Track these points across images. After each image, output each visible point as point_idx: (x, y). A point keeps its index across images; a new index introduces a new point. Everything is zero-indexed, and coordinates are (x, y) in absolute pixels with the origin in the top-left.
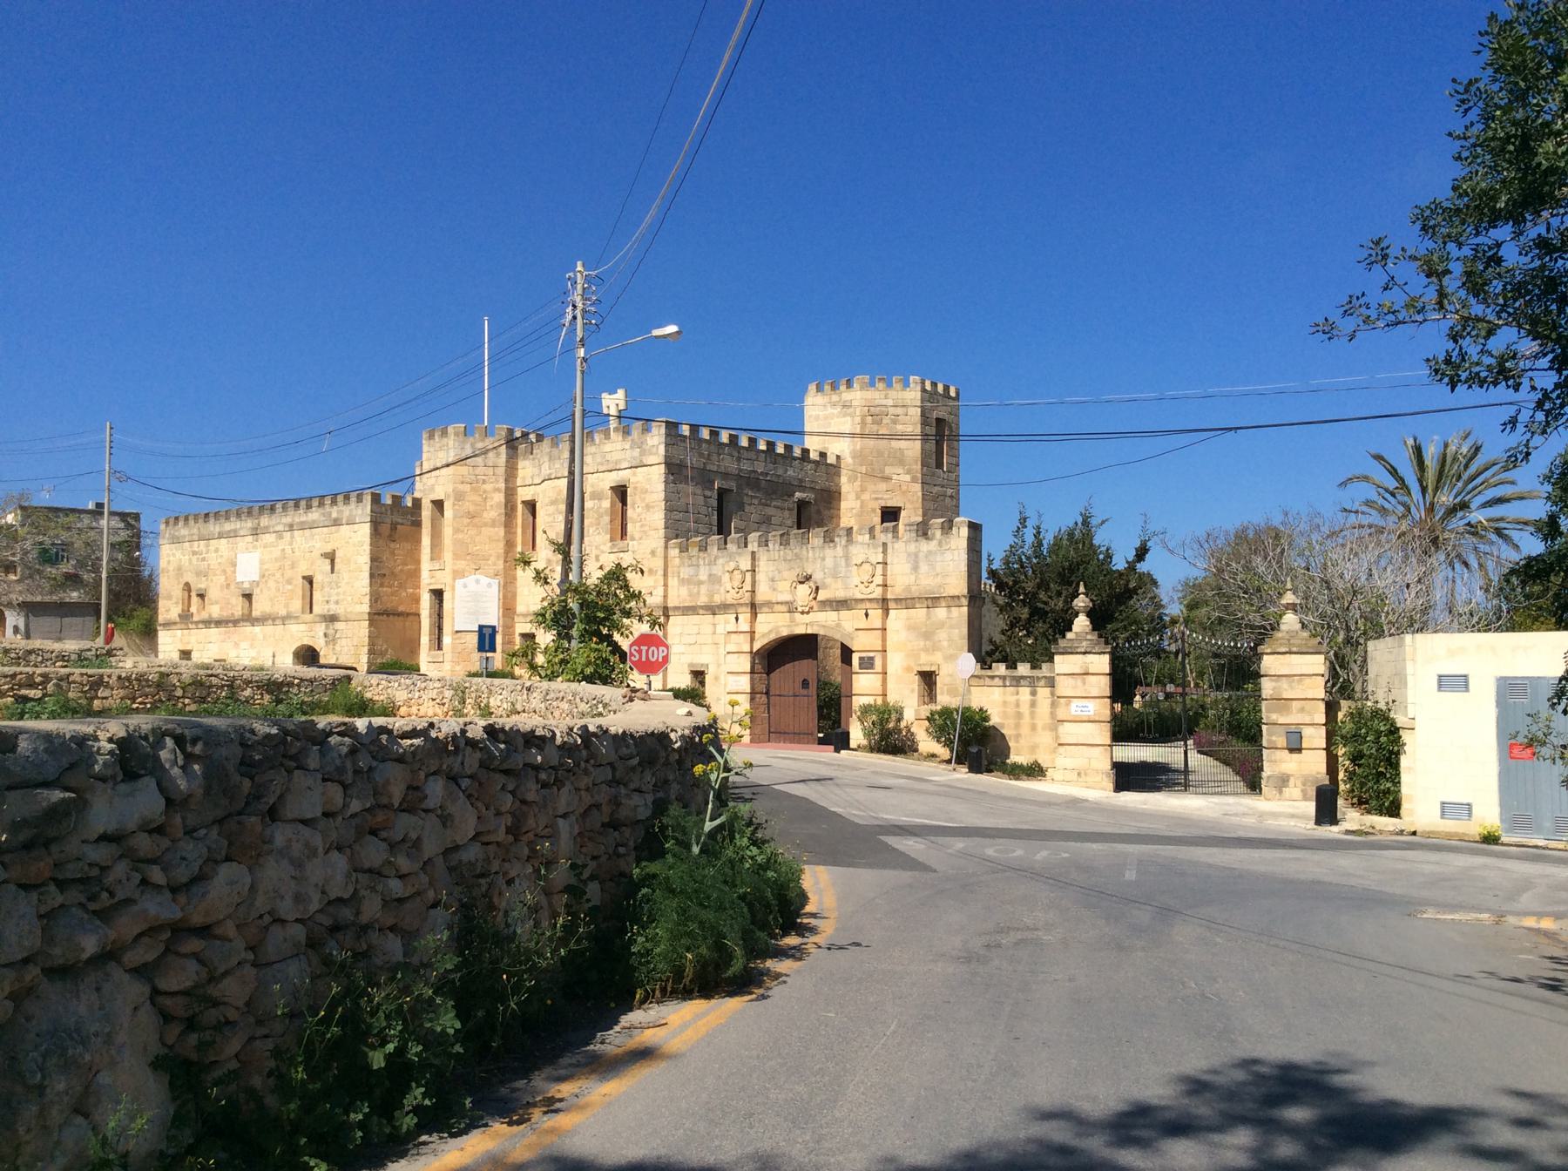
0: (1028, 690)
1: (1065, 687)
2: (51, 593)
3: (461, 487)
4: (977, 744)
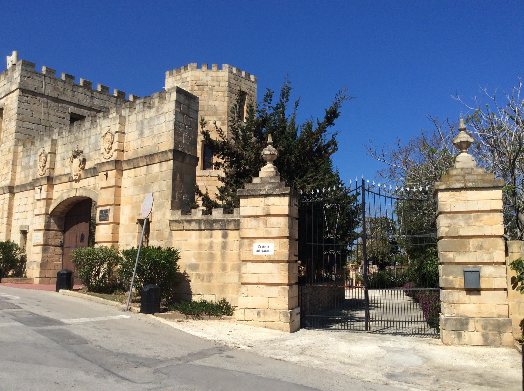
0: (220, 233)
1: (249, 228)
4: (160, 284)
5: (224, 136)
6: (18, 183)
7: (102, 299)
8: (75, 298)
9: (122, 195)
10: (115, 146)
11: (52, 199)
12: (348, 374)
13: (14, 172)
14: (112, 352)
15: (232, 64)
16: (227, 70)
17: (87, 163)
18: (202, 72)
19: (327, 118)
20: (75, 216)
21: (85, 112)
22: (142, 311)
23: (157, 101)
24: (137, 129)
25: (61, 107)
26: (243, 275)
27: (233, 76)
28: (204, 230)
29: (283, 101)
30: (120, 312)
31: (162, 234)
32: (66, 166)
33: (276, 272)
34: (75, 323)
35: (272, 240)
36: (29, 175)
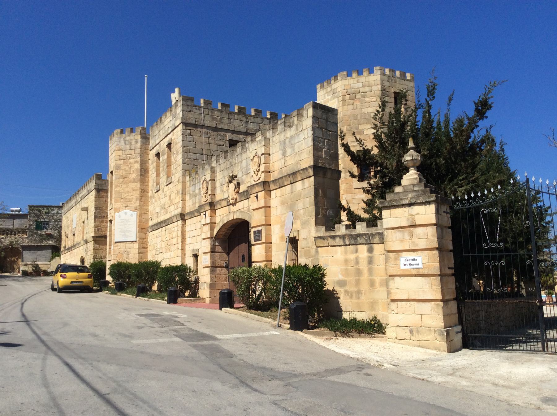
0: (365, 247)
1: (394, 240)
2: (41, 242)
3: (119, 162)
4: (308, 302)
5: (364, 146)
6: (187, 210)
7: (257, 316)
8: (236, 315)
9: (272, 215)
10: (262, 168)
11: (215, 223)
12: (496, 396)
13: (183, 200)
14: (252, 365)
15: (383, 66)
16: (379, 72)
17: (241, 186)
18: (352, 80)
19: (477, 110)
20: (235, 237)
21: (241, 137)
22: (291, 328)
23: (295, 119)
24: (280, 149)
25: (220, 135)
26: (392, 291)
27: (386, 78)
28: (349, 245)
29: (428, 99)
30: (271, 328)
31: (309, 251)
32: (224, 191)
33: (427, 287)
34: (227, 339)
35: (419, 253)
36: (196, 203)
